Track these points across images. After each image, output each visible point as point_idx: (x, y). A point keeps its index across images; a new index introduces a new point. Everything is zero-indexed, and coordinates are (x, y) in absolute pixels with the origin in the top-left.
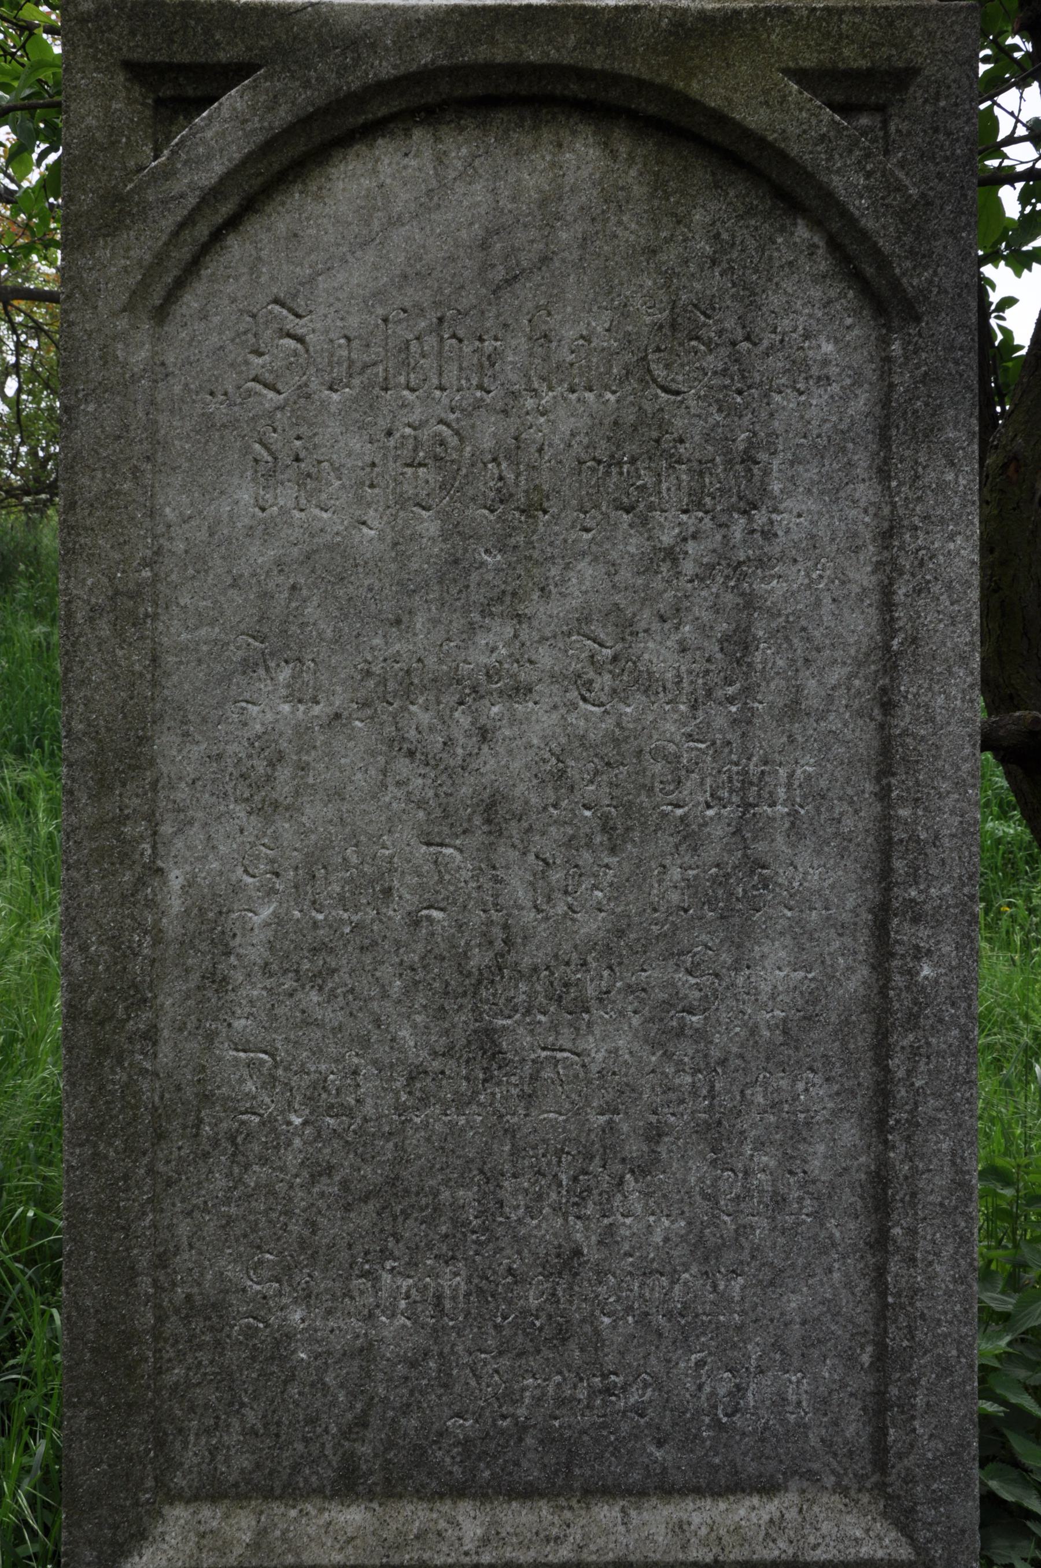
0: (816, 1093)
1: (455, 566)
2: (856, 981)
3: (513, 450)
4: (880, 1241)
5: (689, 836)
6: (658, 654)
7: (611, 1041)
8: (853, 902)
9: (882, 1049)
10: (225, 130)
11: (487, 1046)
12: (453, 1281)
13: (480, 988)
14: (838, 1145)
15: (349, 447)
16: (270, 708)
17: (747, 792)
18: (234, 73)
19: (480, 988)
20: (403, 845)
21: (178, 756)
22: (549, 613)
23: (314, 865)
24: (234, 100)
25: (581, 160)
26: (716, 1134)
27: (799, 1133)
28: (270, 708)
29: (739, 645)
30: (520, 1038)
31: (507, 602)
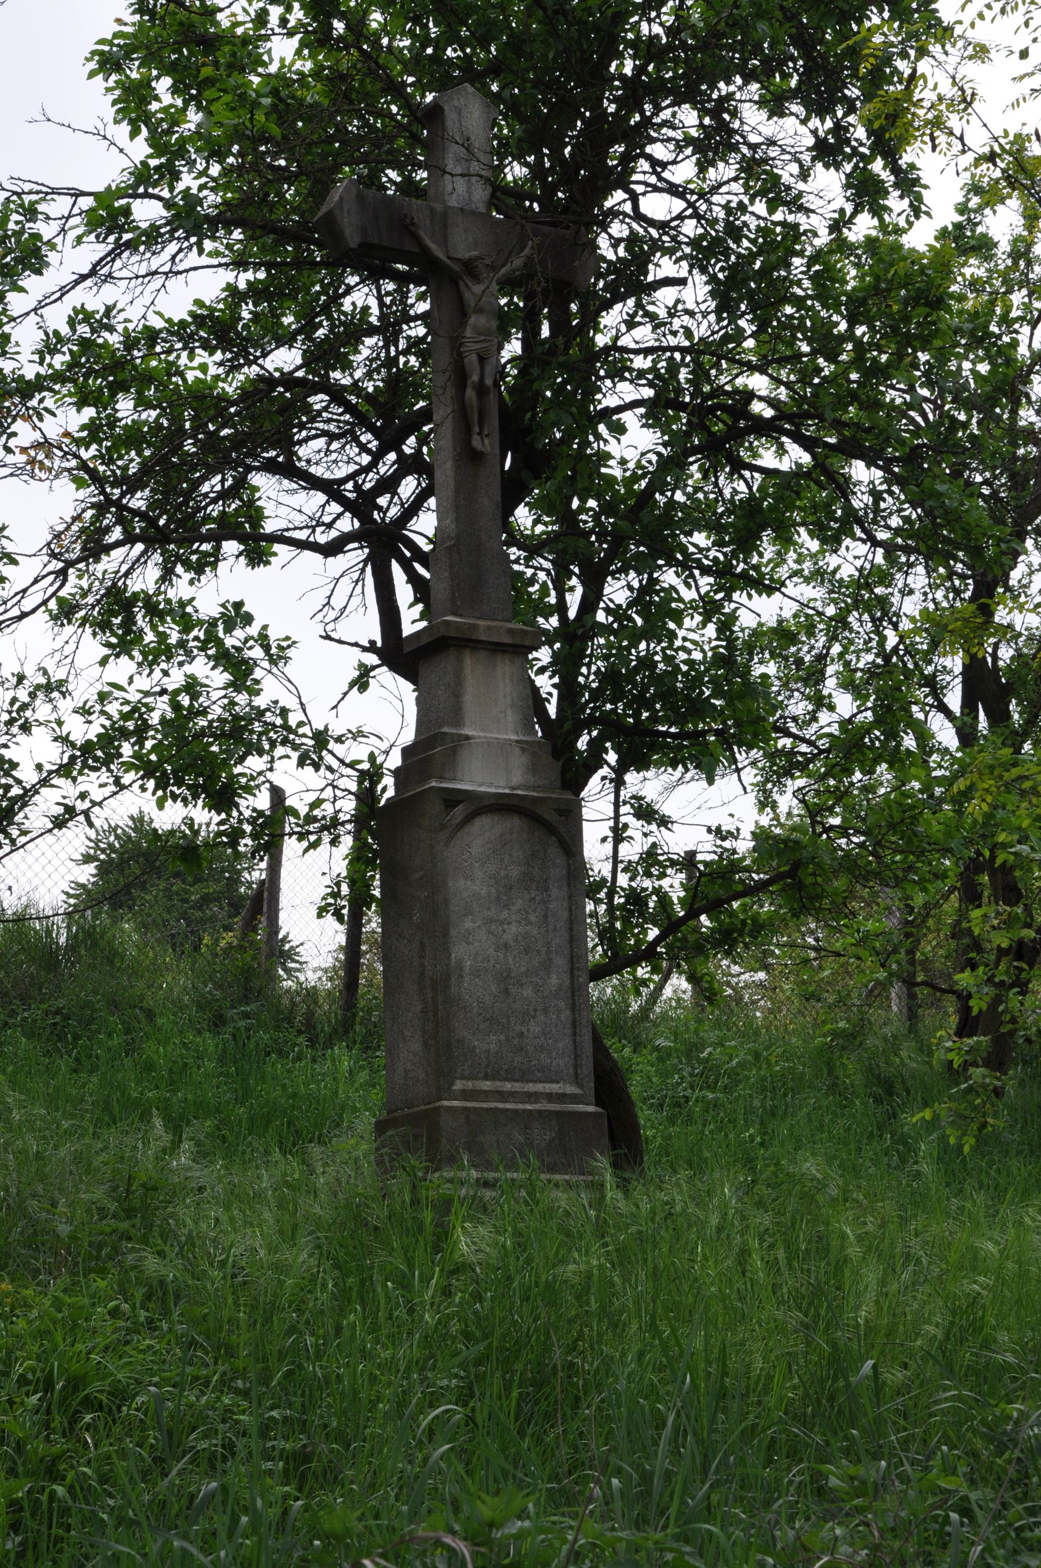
0: (562, 1004)
1: (498, 899)
2: (568, 983)
3: (507, 876)
4: (574, 1034)
5: (539, 952)
6: (532, 918)
7: (527, 992)
8: (567, 968)
9: (573, 996)
10: (459, 812)
11: (506, 991)
12: (502, 1037)
13: (505, 979)
14: (566, 1015)
15: (479, 874)
16: (468, 924)
17: (548, 945)
18: (459, 802)
19: (505, 979)
20: (491, 951)
21: (453, 932)
22: (514, 908)
23: (477, 954)
24: (460, 807)
25: (515, 822)
26: (546, 1011)
27: (559, 1011)
28: (468, 924)
29: (546, 916)
30: (512, 990)
31: (506, 906)
